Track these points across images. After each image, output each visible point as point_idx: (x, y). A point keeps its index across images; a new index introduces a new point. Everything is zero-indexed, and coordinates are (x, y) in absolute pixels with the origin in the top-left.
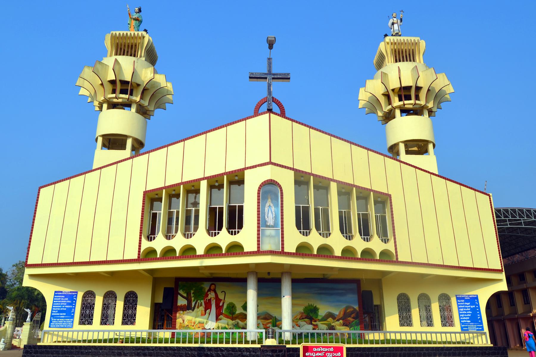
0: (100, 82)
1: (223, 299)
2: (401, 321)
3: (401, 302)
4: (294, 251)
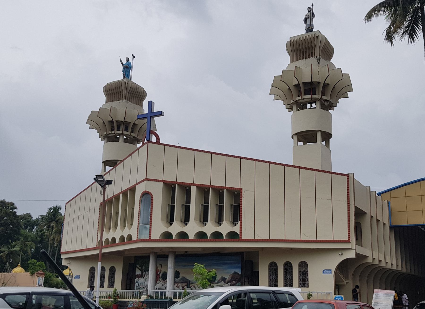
0: (288, 87)
1: (160, 270)
2: (301, 283)
3: (287, 268)
4: (158, 238)
